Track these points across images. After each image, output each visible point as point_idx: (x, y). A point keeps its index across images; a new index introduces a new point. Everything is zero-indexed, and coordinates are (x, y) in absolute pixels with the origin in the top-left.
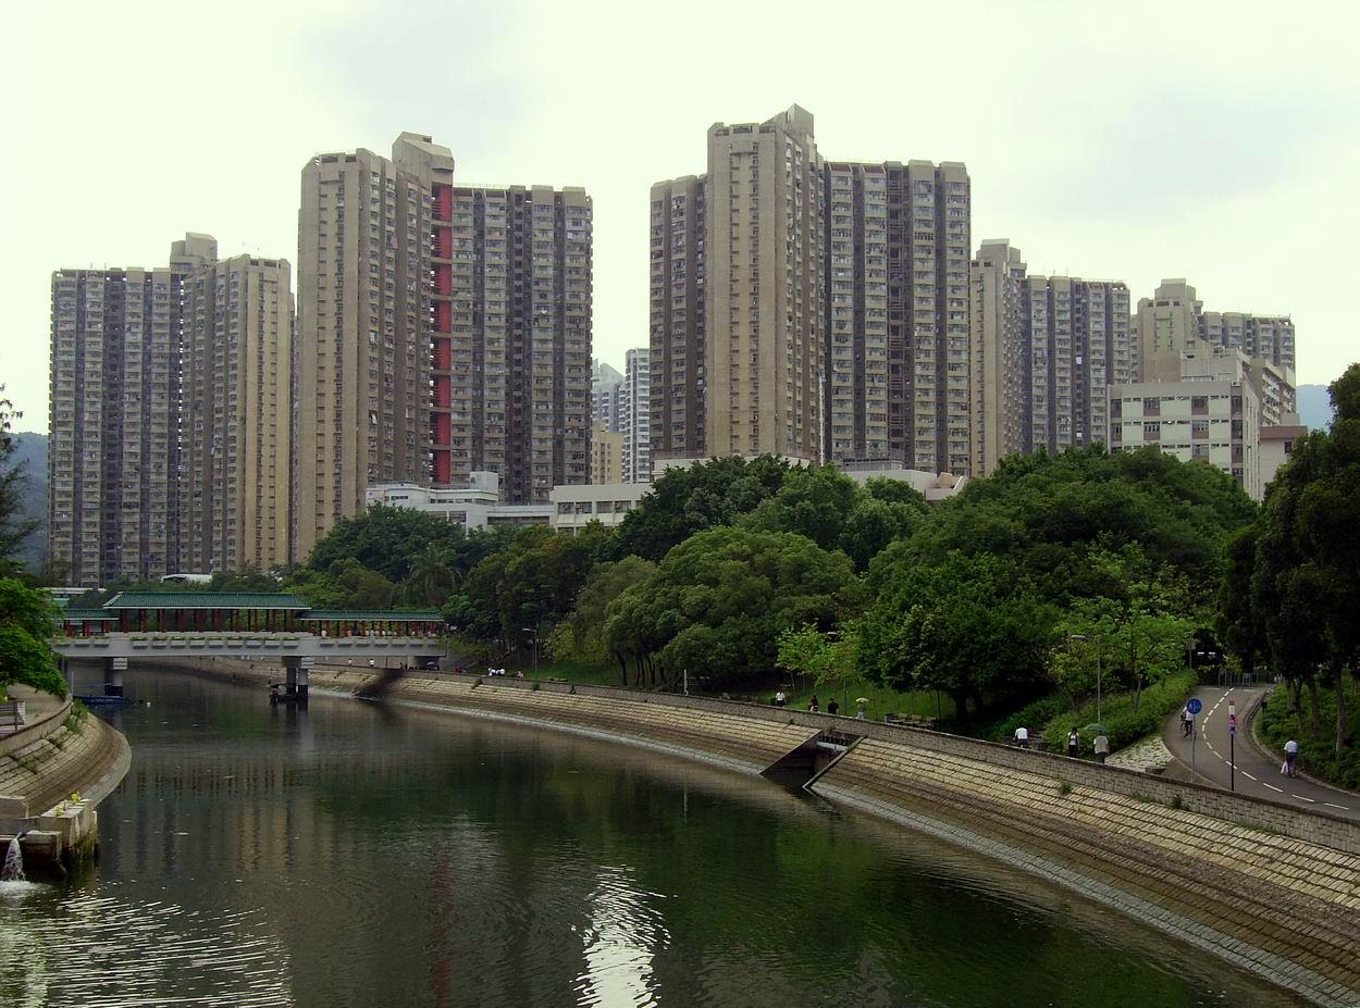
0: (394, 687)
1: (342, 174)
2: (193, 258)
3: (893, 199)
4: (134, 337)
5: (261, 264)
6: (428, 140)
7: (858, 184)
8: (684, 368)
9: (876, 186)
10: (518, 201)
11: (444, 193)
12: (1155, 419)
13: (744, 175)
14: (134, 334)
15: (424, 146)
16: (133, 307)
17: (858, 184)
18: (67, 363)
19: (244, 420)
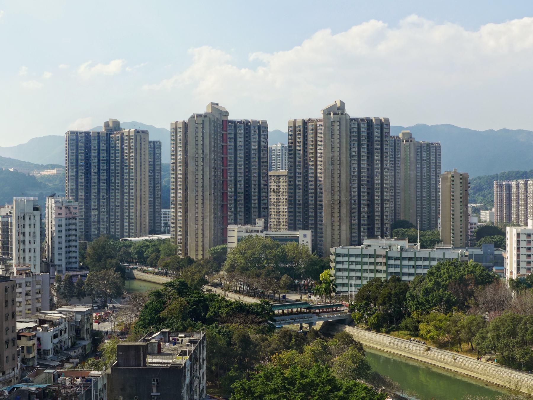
0: (340, 328)
1: (203, 121)
2: (113, 128)
3: (368, 129)
4: (94, 153)
5: (141, 132)
6: (217, 104)
7: (359, 125)
8: (301, 179)
9: (364, 126)
10: (247, 126)
11: (226, 124)
12: (530, 239)
13: (337, 128)
14: (241, 216)
15: (216, 106)
16: (94, 143)
17: (359, 125)
18: (72, 163)
19: (136, 183)
